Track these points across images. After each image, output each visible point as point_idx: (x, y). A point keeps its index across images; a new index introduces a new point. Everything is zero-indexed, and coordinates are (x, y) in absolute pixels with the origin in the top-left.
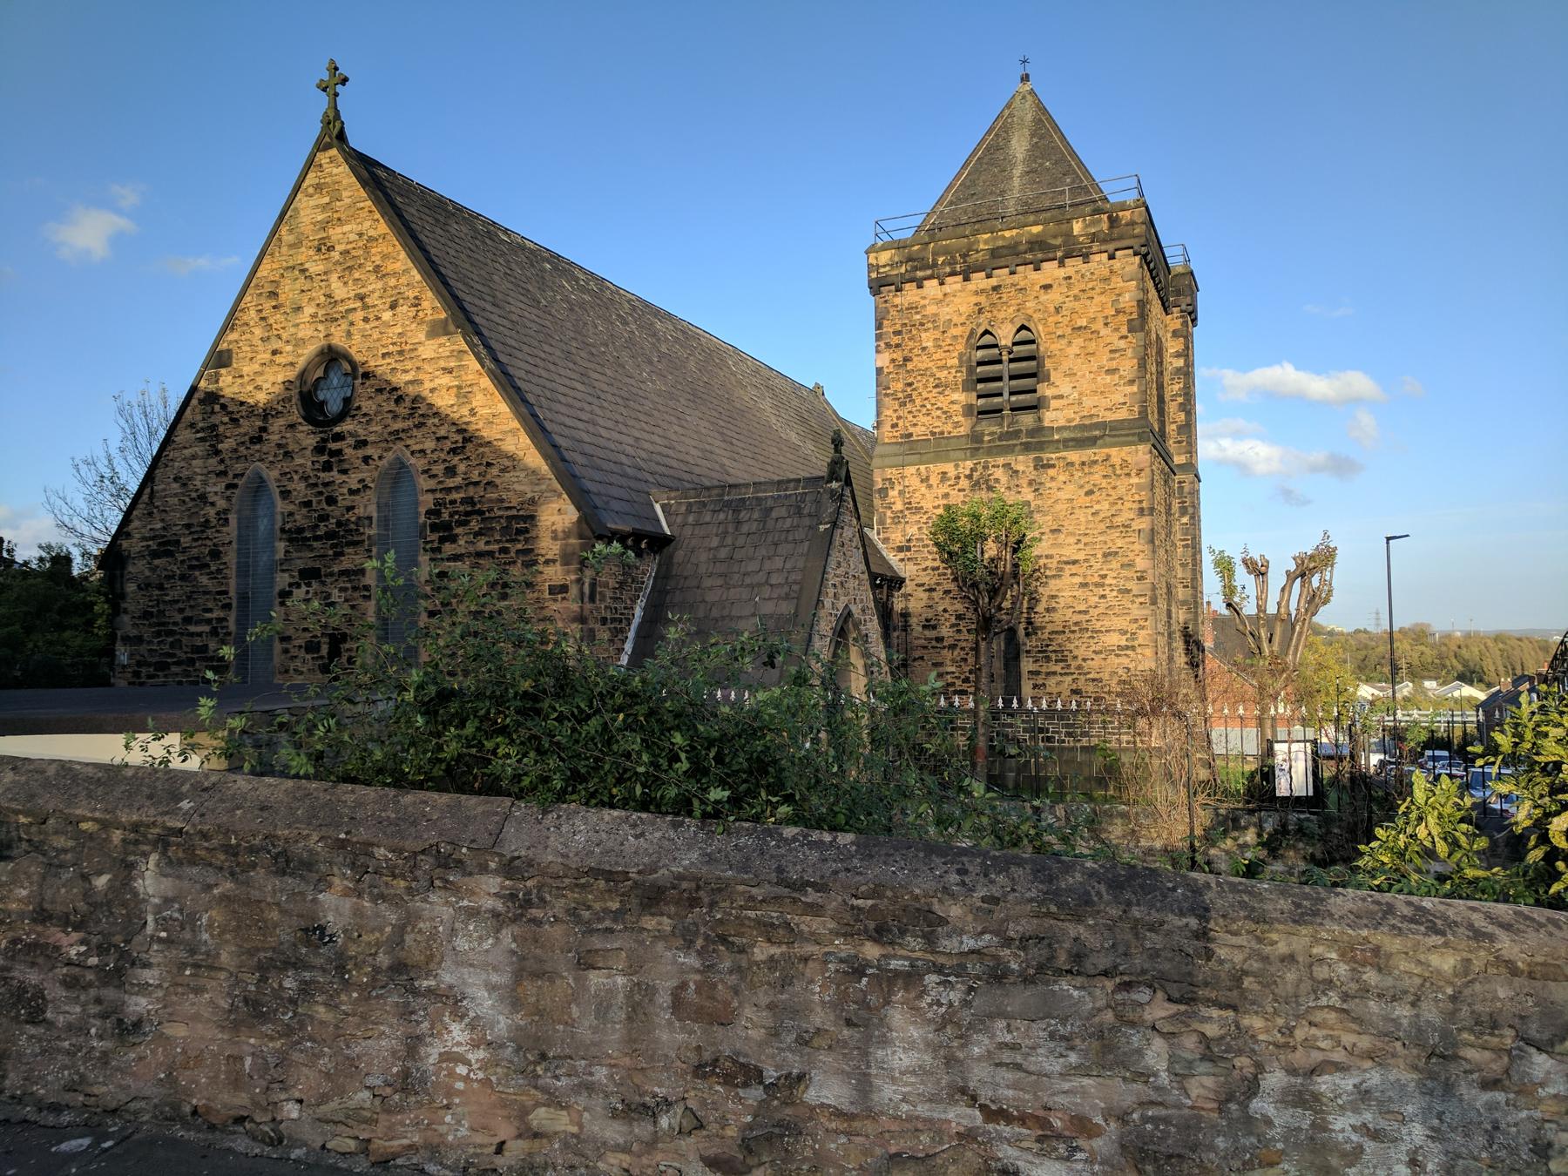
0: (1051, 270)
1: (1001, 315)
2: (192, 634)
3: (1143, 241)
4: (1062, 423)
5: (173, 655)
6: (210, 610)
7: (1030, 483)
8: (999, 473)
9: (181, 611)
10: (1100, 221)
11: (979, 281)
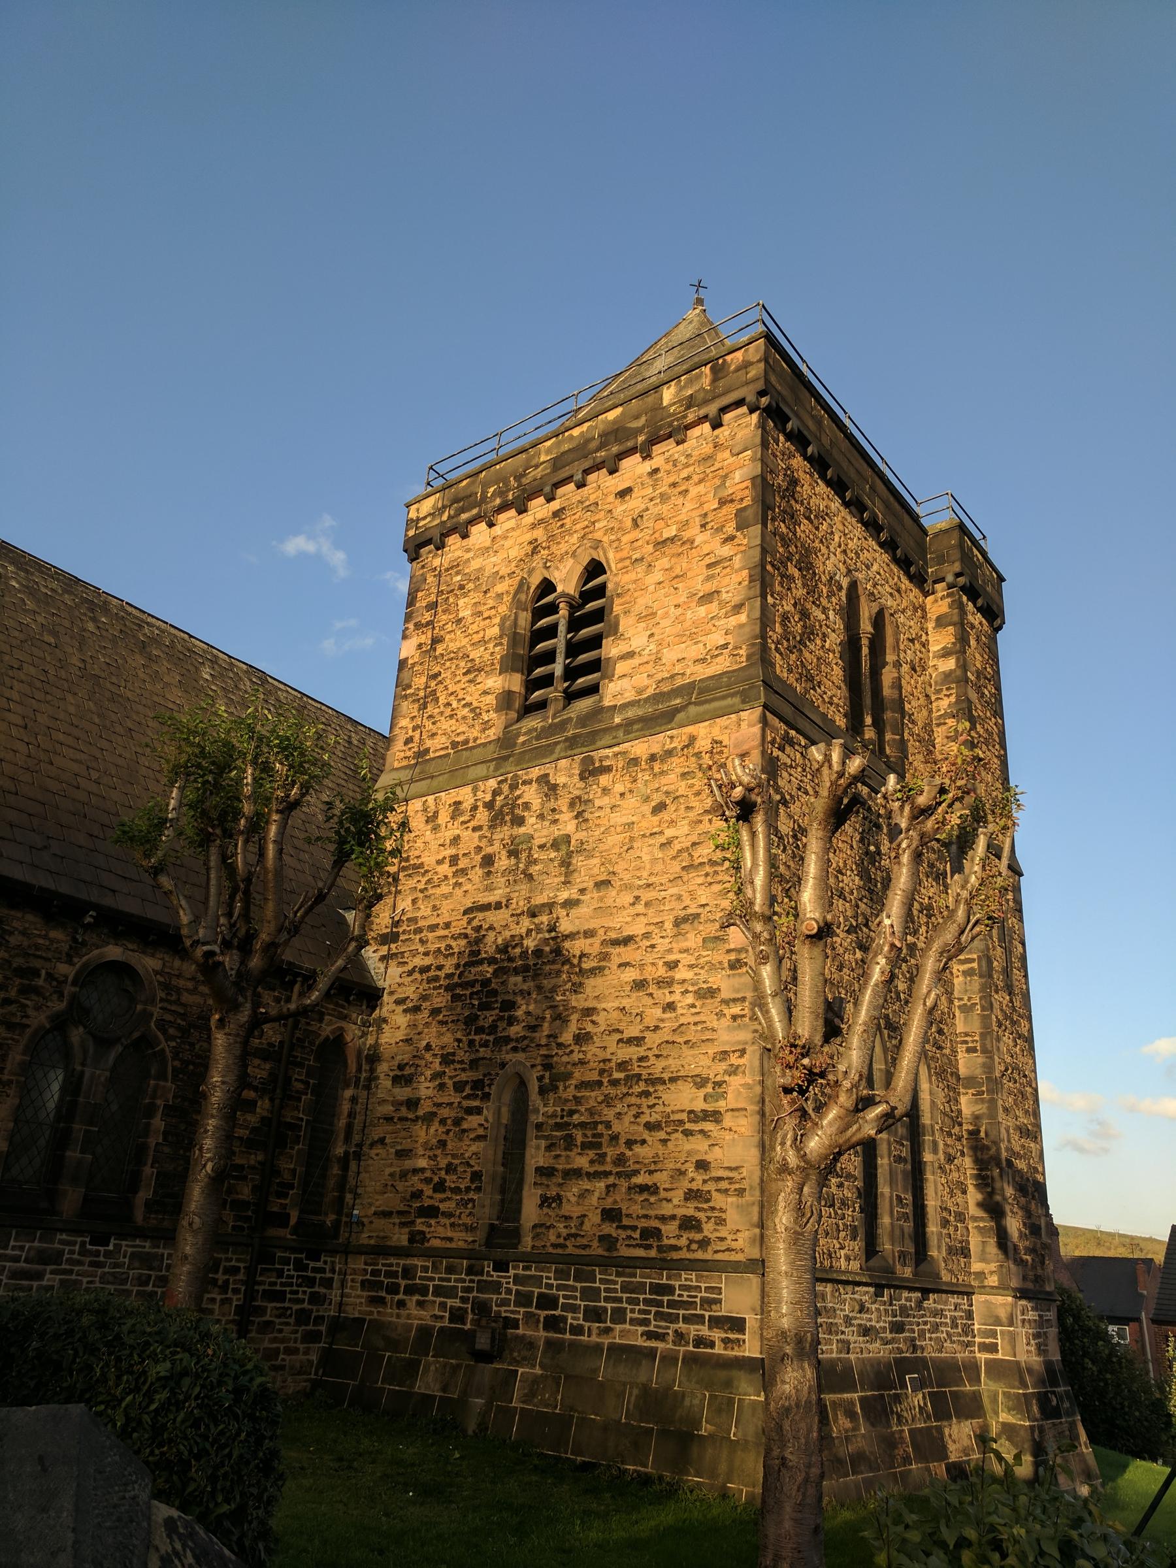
0: (634, 467)
1: (564, 547)
3: (760, 385)
4: (630, 696)
7: (572, 805)
8: (531, 795)
10: (699, 377)
11: (539, 508)
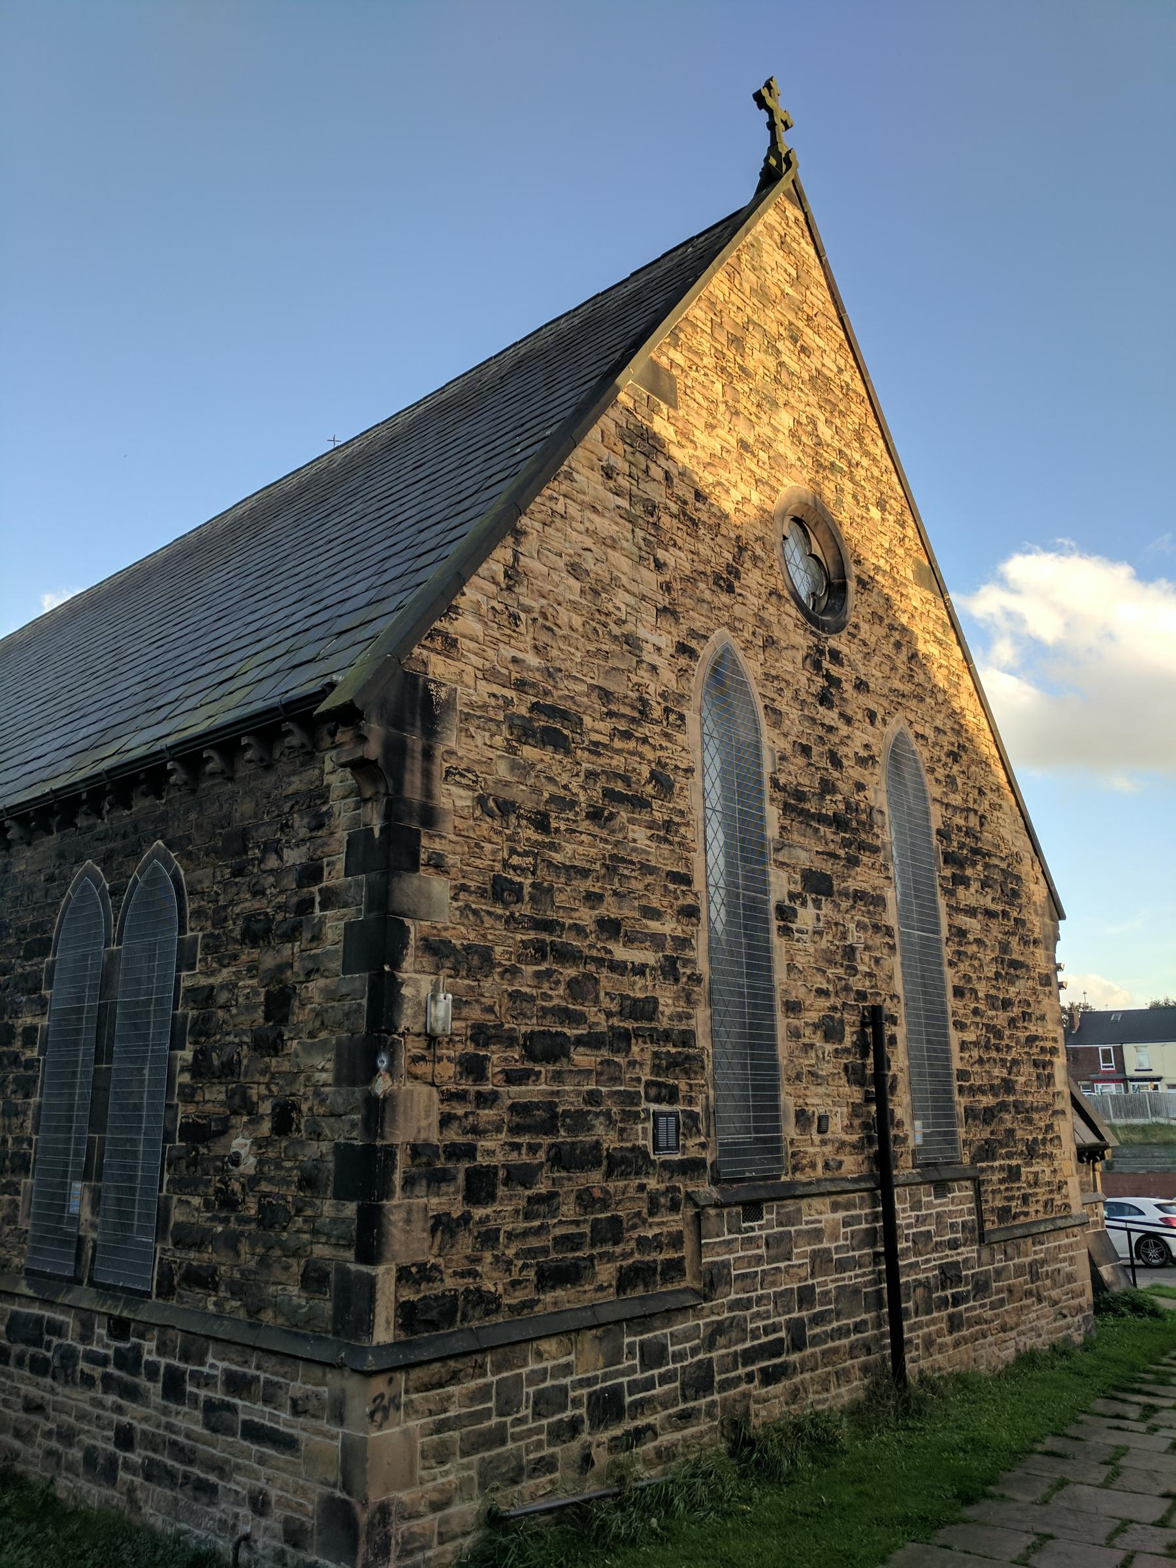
2: (618, 967)
5: (577, 1018)
6: (655, 914)
9: (593, 899)
